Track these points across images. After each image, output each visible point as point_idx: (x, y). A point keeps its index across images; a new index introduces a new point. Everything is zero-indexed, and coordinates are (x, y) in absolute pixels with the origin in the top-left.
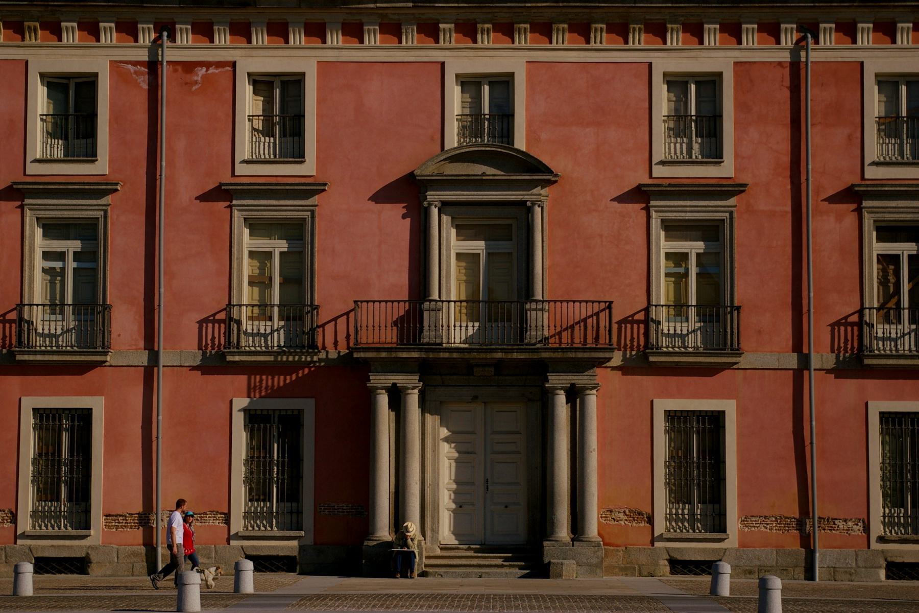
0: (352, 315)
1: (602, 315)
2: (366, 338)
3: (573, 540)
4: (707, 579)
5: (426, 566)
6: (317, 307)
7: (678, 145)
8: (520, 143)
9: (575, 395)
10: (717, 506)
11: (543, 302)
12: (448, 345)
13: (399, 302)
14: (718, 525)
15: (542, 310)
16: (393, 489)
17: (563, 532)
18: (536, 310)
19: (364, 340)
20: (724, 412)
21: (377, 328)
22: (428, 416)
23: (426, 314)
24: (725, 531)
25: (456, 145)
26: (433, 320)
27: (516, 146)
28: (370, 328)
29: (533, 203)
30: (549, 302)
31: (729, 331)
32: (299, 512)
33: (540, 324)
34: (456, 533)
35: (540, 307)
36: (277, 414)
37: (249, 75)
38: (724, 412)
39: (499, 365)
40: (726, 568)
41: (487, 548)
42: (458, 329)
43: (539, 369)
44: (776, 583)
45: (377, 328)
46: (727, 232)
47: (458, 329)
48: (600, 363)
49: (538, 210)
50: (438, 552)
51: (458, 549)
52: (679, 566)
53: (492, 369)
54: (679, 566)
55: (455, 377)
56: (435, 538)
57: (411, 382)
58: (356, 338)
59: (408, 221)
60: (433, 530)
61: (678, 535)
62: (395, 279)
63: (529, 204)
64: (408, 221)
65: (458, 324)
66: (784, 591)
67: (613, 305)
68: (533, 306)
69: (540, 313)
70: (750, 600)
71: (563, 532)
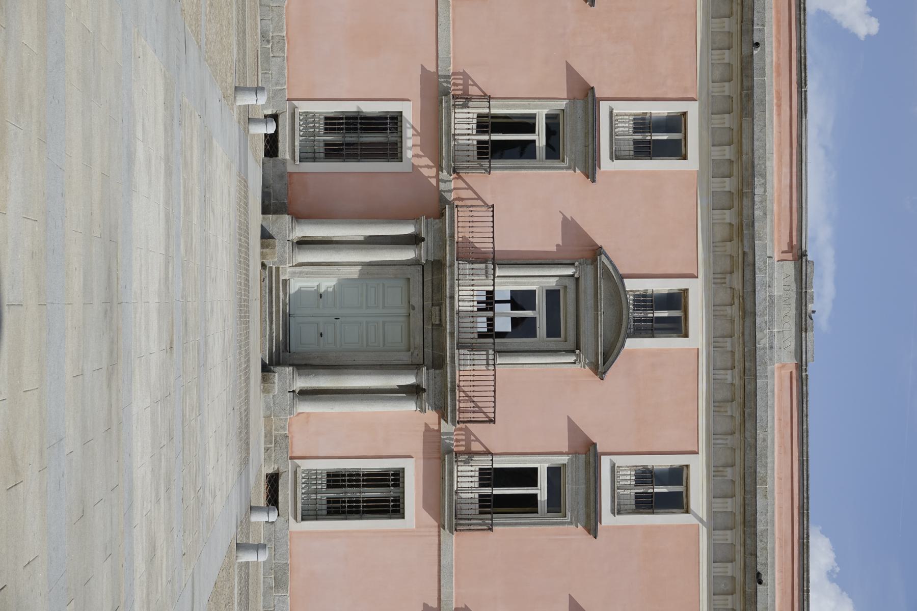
0: (479, 203)
1: (482, 415)
2: (462, 216)
3: (293, 391)
4: (263, 502)
5: (271, 268)
6: (491, 529)
7: (628, 478)
8: (632, 344)
9: (414, 391)
10: (325, 512)
11: (494, 365)
12: (456, 286)
13: (493, 243)
14: (309, 515)
15: (488, 364)
16: (334, 239)
17: (303, 383)
18: (487, 359)
19: (461, 214)
20: (403, 518)
21: (471, 224)
22: (359, 268)
23: (483, 266)
24: (303, 520)
25: (627, 289)
26: (479, 272)
27: (628, 341)
28: (472, 219)
29: (577, 355)
30: (494, 370)
31: (472, 522)
32: (314, 160)
33: (476, 362)
34: (299, 291)
35: (491, 362)
36: (399, 140)
37: (685, 114)
38: (403, 518)
39: (441, 326)
40: (273, 517)
41: (287, 318)
42: (471, 293)
43: (438, 363)
44: (263, 557)
45: (471, 224)
46: (555, 520)
47: (471, 293)
48: (443, 416)
49: (572, 359)
50: (282, 278)
51: (285, 294)
52: (273, 481)
53: (437, 322)
54: (273, 481)
55: (430, 290)
56: (294, 274)
57: (423, 253)
58: (462, 206)
59: (554, 249)
60: (301, 273)
61: (300, 480)
62: (506, 243)
63: (577, 352)
64: (554, 249)
65: (475, 293)
66: (257, 563)
67: (492, 424)
68: (491, 357)
69: (485, 362)
70: (248, 538)
71: (303, 383)
